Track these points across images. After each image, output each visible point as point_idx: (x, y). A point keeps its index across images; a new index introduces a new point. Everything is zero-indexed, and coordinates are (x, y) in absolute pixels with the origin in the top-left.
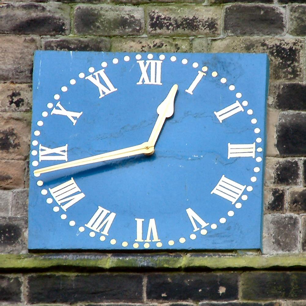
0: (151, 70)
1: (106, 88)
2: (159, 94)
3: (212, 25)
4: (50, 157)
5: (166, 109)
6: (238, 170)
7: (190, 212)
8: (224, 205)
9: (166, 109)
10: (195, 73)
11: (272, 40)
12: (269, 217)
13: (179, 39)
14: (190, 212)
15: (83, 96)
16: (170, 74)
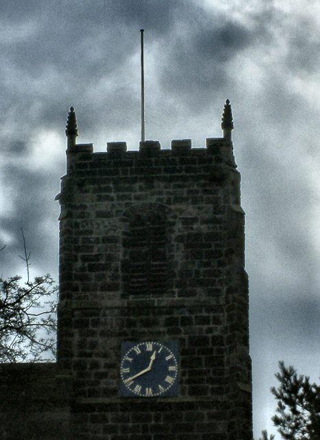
0: (149, 347)
1: (138, 352)
2: (151, 353)
3: (164, 332)
4: (128, 381)
5: (153, 357)
6: (172, 374)
7: (160, 386)
8: (168, 384)
9: (153, 357)
10: (160, 347)
11: (179, 336)
12: (179, 386)
13: (169, 397)
14: (160, 386)
15: (133, 354)
16: (156, 348)
